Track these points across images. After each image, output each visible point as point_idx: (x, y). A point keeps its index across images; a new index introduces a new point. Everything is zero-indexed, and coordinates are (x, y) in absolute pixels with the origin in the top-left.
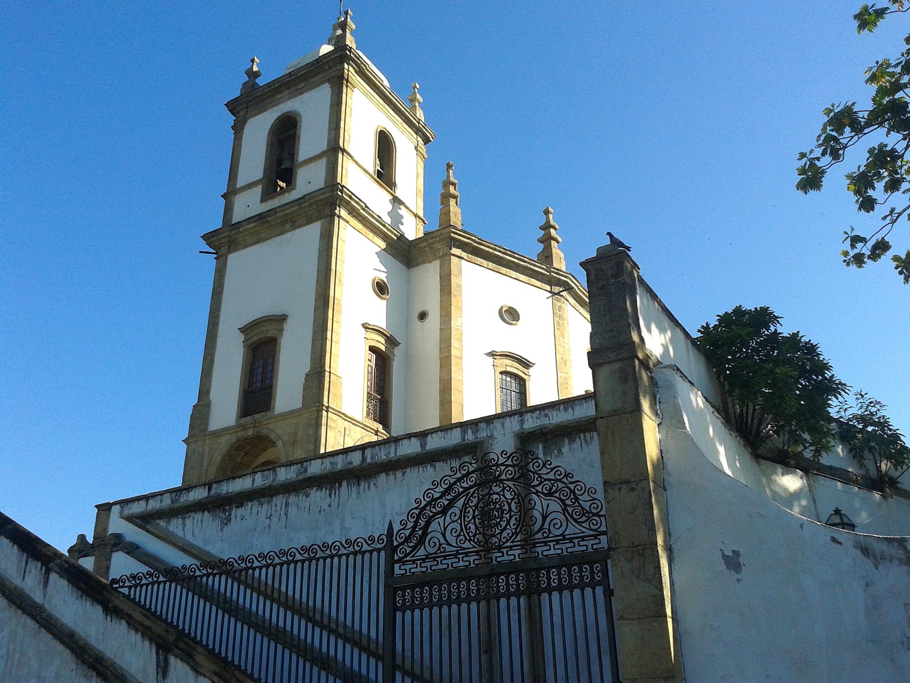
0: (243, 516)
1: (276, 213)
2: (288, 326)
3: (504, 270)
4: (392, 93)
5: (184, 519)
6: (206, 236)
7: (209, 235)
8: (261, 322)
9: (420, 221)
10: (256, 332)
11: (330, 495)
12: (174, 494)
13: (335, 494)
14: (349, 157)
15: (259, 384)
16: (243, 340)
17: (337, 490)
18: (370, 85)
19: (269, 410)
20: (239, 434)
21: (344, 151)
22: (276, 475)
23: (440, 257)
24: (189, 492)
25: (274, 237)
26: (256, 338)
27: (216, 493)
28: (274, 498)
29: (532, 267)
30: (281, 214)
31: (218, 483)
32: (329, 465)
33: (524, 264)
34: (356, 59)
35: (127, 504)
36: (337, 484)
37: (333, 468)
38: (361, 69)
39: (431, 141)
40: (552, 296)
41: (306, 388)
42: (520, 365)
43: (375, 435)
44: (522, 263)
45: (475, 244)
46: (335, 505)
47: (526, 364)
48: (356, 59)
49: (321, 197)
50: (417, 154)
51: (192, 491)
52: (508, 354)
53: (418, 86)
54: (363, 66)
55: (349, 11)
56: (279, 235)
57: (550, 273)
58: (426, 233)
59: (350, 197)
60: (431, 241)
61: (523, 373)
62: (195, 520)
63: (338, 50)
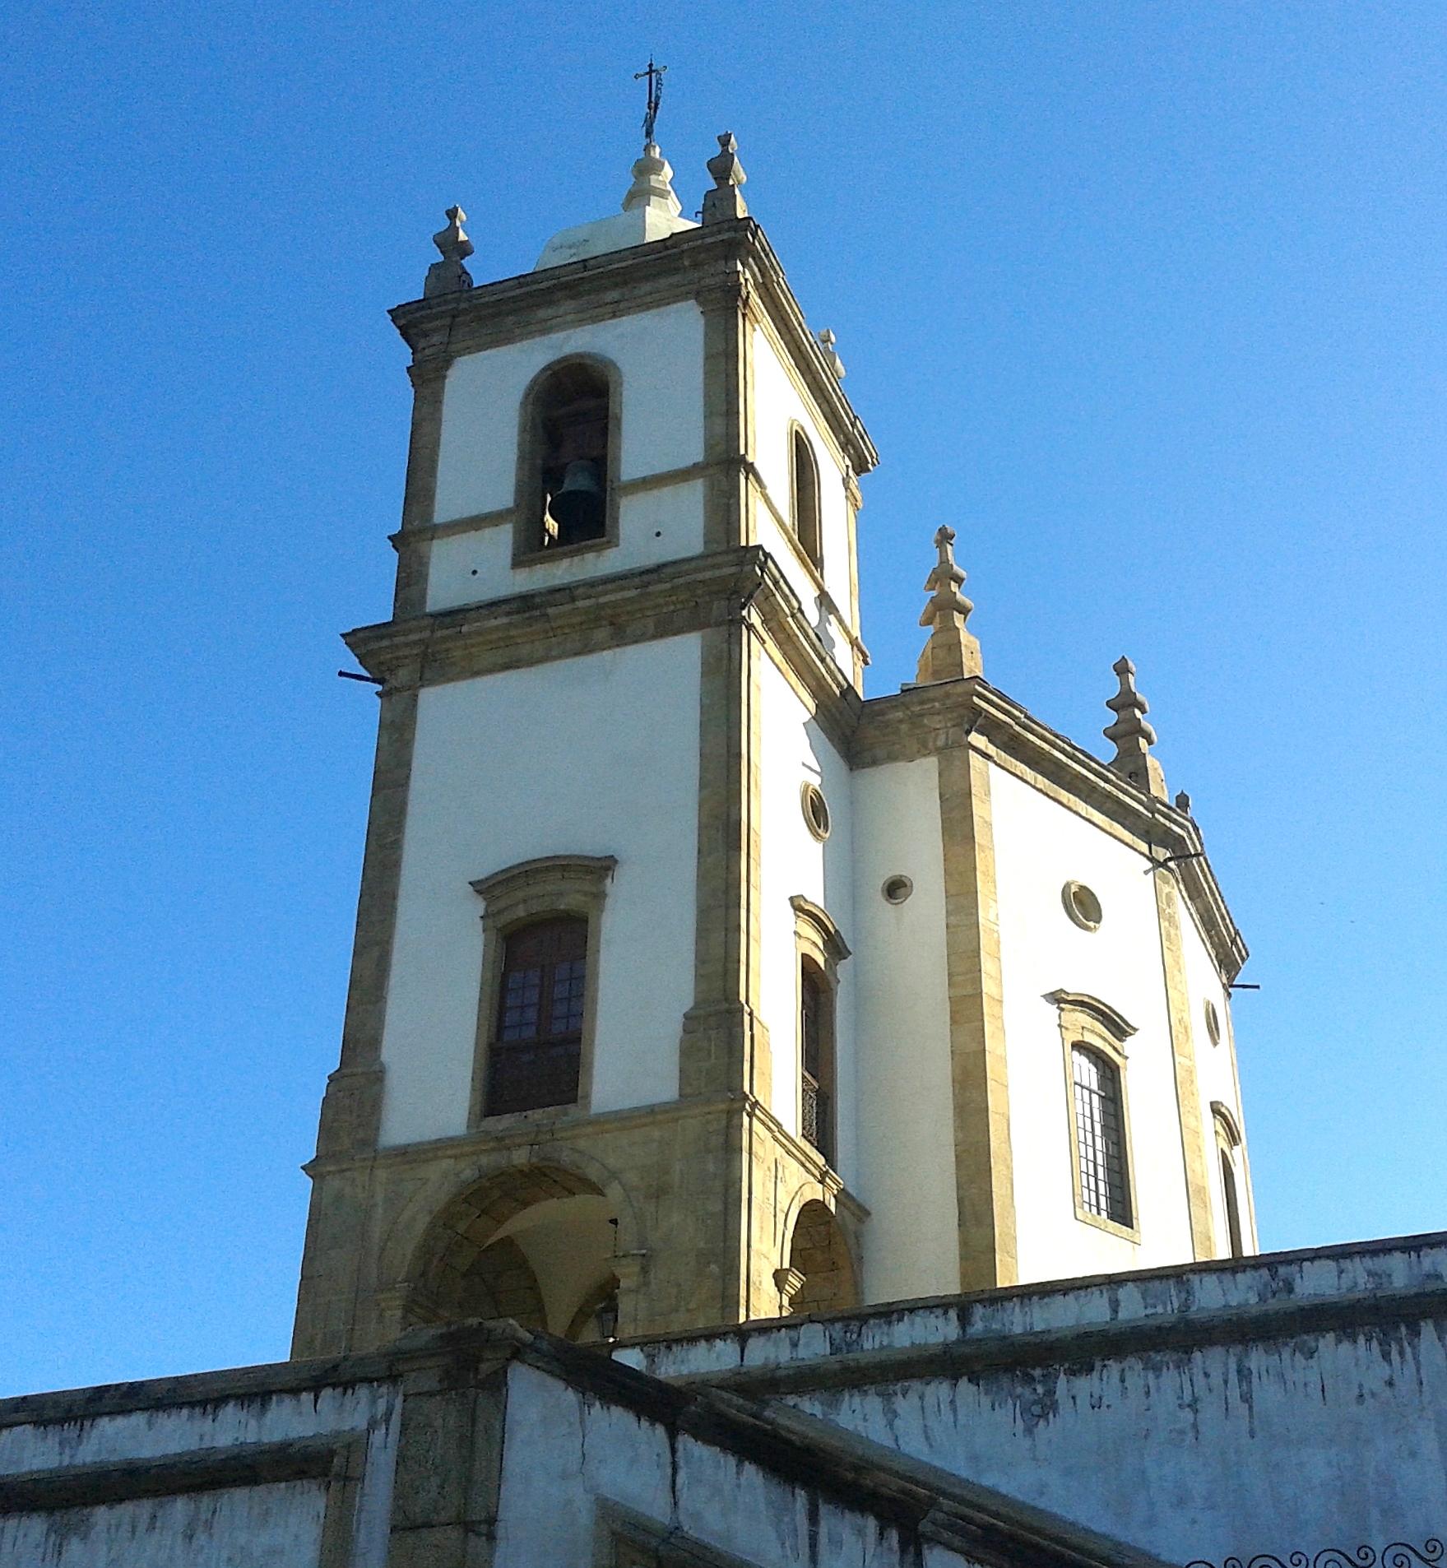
0: (1096, 1396)
1: (573, 600)
2: (618, 888)
3: (1064, 796)
4: (815, 347)
5: (887, 1397)
6: (360, 635)
7: (367, 633)
8: (537, 871)
9: (860, 655)
10: (520, 894)
11: (1386, 1356)
12: (838, 1326)
13: (1402, 1353)
14: (757, 485)
15: (529, 1033)
16: (482, 913)
17: (1406, 1344)
18: (777, 321)
19: (574, 1100)
20: (484, 1160)
21: (750, 469)
22: (1188, 1292)
23: (939, 751)
24: (890, 1323)
25: (555, 658)
26: (521, 912)
27: (987, 1329)
28: (1197, 1355)
29: (1121, 795)
30: (587, 603)
31: (991, 1305)
32: (1363, 1280)
33: (1108, 787)
34: (762, 254)
35: (669, 1348)
36: (1403, 1329)
37: (1379, 1286)
38: (768, 281)
39: (869, 470)
40: (1154, 869)
41: (687, 1053)
42: (1106, 1027)
43: (820, 1182)
44: (1102, 784)
45: (1017, 728)
46: (1405, 1385)
47: (1119, 1028)
48: (762, 254)
49: (708, 575)
50: (847, 497)
51: (900, 1320)
52: (1086, 999)
53: (833, 338)
54: (772, 273)
55: (733, 139)
56: (576, 654)
57: (1153, 813)
58: (905, 688)
59: (776, 583)
60: (917, 709)
61: (1115, 1049)
62: (930, 1400)
63: (707, 230)
